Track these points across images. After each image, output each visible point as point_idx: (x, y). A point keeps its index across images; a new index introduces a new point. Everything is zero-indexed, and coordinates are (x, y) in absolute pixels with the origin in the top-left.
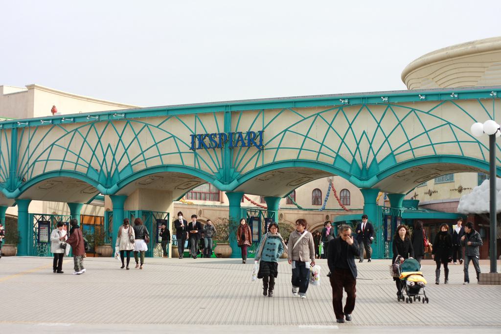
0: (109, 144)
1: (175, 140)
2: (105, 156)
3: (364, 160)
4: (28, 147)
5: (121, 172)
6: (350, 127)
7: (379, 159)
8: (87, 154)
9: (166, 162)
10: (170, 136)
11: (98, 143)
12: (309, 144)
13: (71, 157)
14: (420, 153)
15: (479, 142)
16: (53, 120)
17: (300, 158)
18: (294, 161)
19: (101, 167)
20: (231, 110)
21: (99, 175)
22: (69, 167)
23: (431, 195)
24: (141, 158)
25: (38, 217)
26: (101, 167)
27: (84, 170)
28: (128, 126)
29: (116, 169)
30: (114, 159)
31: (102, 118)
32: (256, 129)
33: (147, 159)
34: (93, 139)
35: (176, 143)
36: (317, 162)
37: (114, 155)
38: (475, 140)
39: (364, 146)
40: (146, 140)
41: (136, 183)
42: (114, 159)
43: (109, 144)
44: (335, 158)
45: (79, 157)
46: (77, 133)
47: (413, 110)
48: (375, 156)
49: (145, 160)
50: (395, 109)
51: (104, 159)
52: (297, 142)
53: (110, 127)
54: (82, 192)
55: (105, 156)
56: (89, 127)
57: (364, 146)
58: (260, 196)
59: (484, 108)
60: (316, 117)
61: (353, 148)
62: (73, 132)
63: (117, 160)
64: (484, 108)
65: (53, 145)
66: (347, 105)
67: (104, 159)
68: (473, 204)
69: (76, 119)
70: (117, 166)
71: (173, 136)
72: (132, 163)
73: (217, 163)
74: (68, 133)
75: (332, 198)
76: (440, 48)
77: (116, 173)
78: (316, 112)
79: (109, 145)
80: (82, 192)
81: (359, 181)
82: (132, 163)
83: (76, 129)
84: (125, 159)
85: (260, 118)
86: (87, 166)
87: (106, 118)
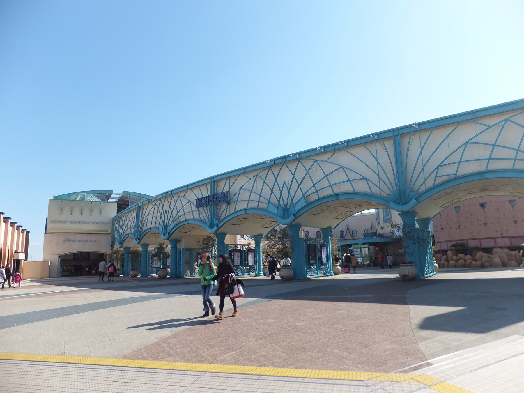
0: (284, 182)
1: (343, 169)
2: (281, 192)
3: (285, 204)
5: (296, 204)
7: (295, 201)
8: (267, 192)
10: (337, 167)
11: (176, 202)
12: (498, 153)
14: (322, 194)
15: (366, 179)
17: (515, 167)
18: (245, 210)
19: (279, 201)
20: (213, 181)
21: (278, 208)
23: (382, 229)
24: (313, 190)
26: (279, 201)
27: (265, 206)
28: (300, 163)
29: (292, 202)
30: (289, 194)
31: (277, 162)
32: (226, 189)
33: (319, 190)
34: (271, 179)
35: (345, 171)
36: (513, 170)
37: (289, 191)
38: (362, 178)
39: (285, 193)
40: (317, 174)
41: (309, 213)
42: (289, 194)
43: (284, 182)
44: (268, 204)
45: (260, 196)
47: (316, 161)
48: (292, 199)
49: (317, 191)
50: (304, 162)
51: (281, 195)
53: (284, 167)
54: (263, 227)
55: (281, 192)
57: (285, 193)
58: (240, 235)
59: (368, 150)
61: (278, 196)
62: (255, 177)
63: (292, 194)
64: (368, 150)
66: (274, 165)
67: (281, 195)
68: (452, 239)
69: (157, 198)
70: (292, 199)
71: (342, 167)
72: (305, 196)
73: (206, 212)
74: (250, 179)
75: (348, 234)
77: (292, 206)
78: (255, 173)
79: (285, 183)
80: (263, 227)
81: (282, 219)
82: (305, 196)
83: (257, 175)
85: (270, 173)
86: (267, 202)
87: (280, 161)
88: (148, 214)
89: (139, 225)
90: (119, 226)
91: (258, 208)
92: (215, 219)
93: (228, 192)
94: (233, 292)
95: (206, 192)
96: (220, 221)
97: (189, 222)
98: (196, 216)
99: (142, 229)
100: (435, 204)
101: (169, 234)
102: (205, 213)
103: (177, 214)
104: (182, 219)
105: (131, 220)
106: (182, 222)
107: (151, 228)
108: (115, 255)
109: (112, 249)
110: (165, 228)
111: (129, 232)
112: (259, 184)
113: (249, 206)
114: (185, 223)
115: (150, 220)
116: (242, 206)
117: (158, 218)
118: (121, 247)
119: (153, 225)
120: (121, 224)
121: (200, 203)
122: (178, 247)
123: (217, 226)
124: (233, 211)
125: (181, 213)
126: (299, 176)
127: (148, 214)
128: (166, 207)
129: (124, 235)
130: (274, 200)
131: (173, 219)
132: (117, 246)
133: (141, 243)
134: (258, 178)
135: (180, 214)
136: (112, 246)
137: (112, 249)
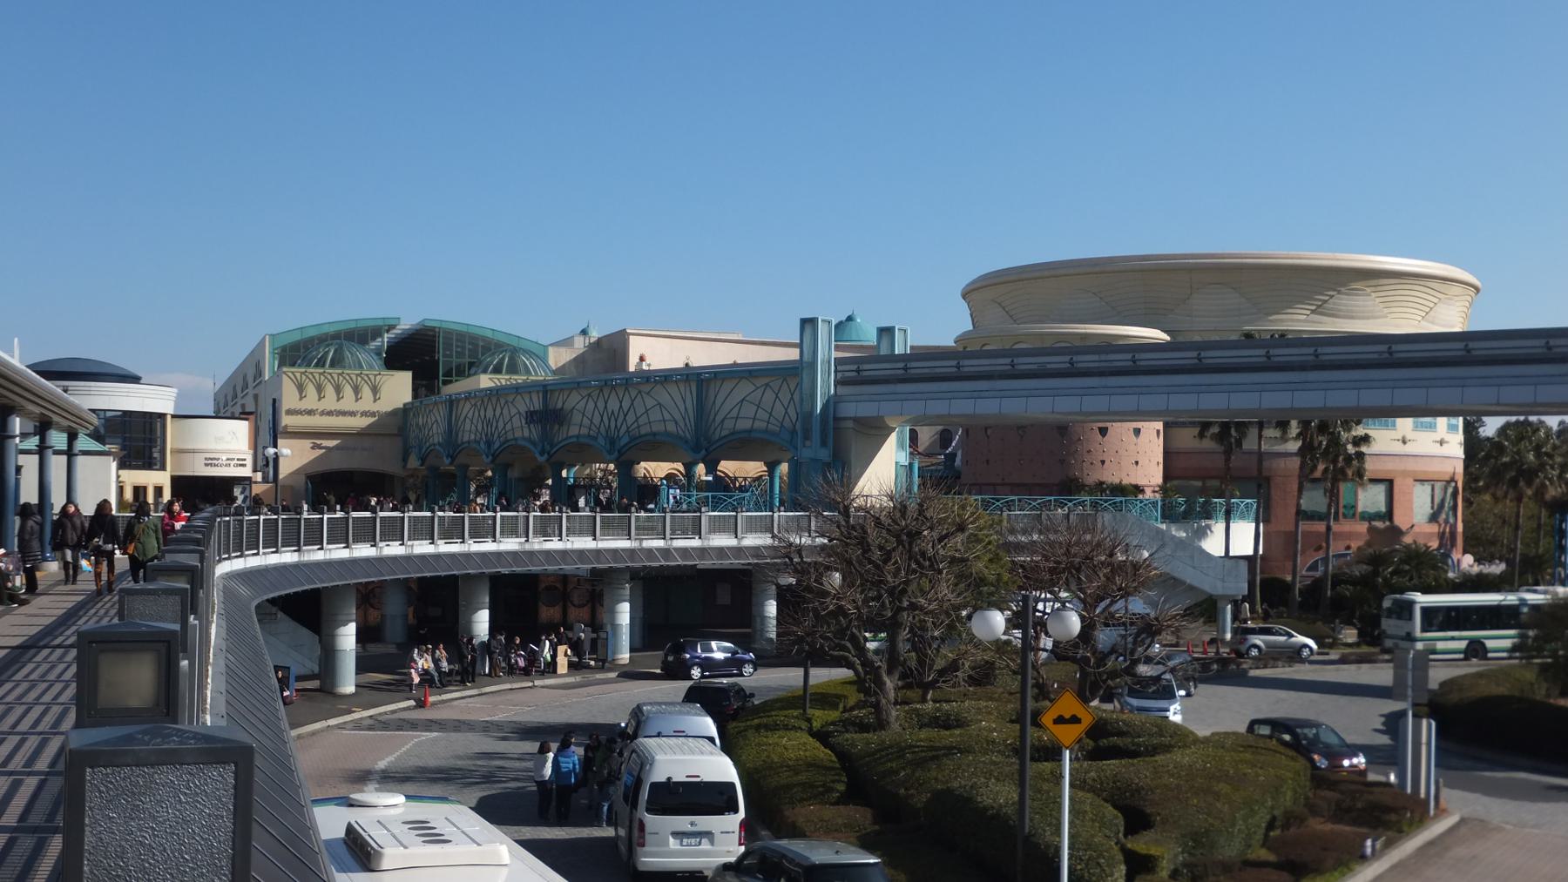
4: (714, 401)
6: (777, 397)
9: (654, 429)
13: (762, 415)
16: (687, 375)
22: (758, 425)
23: (1441, 445)
25: (740, 480)
28: (613, 391)
45: (771, 414)
46: (768, 388)
49: (470, 431)
52: (748, 410)
56: (738, 380)
60: (765, 390)
65: (743, 399)
69: (581, 385)
70: (618, 432)
71: (659, 404)
72: (630, 429)
74: (758, 388)
76: (970, 319)
78: (766, 380)
83: (767, 385)
84: (624, 426)
88: (465, 418)
89: (451, 431)
90: (417, 425)
91: (766, 431)
92: (702, 439)
93: (562, 408)
94: (29, 503)
95: (537, 404)
96: (552, 446)
97: (657, 437)
98: (526, 434)
99: (456, 440)
100: (206, 459)
101: (493, 455)
102: (533, 432)
103: (636, 421)
104: (644, 431)
105: (438, 418)
106: (570, 437)
107: (469, 442)
108: (411, 480)
109: (404, 467)
110: (489, 444)
111: (436, 441)
112: (769, 396)
113: (755, 426)
114: (513, 442)
115: (468, 427)
116: (574, 431)
117: (480, 428)
118: (422, 465)
119: (473, 437)
120: (421, 423)
121: (532, 417)
122: (509, 474)
123: (548, 454)
124: (565, 436)
125: (508, 427)
126: (626, 405)
127: (465, 418)
128: (490, 413)
129: (428, 444)
130: (787, 424)
131: (628, 428)
132: (413, 462)
133: (455, 463)
134: (768, 389)
135: (641, 421)
136: (405, 460)
137: (404, 467)
